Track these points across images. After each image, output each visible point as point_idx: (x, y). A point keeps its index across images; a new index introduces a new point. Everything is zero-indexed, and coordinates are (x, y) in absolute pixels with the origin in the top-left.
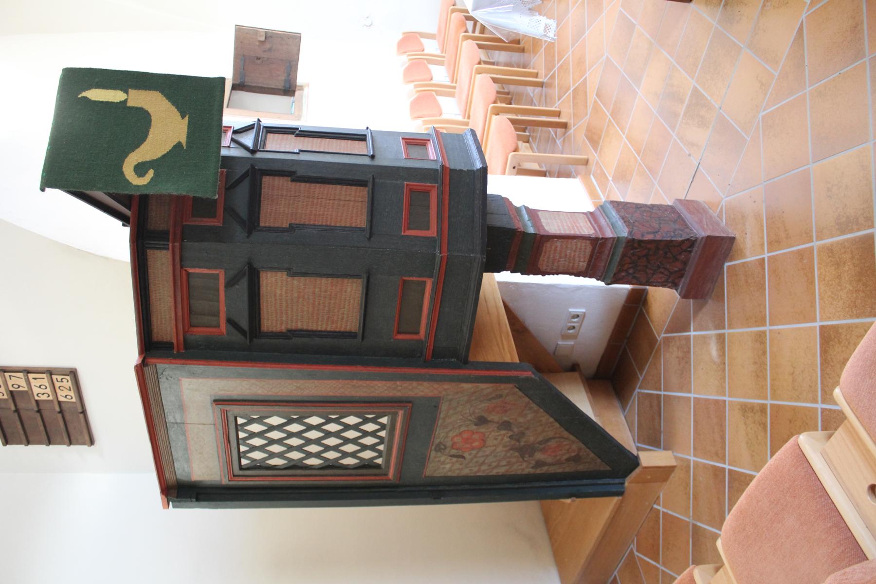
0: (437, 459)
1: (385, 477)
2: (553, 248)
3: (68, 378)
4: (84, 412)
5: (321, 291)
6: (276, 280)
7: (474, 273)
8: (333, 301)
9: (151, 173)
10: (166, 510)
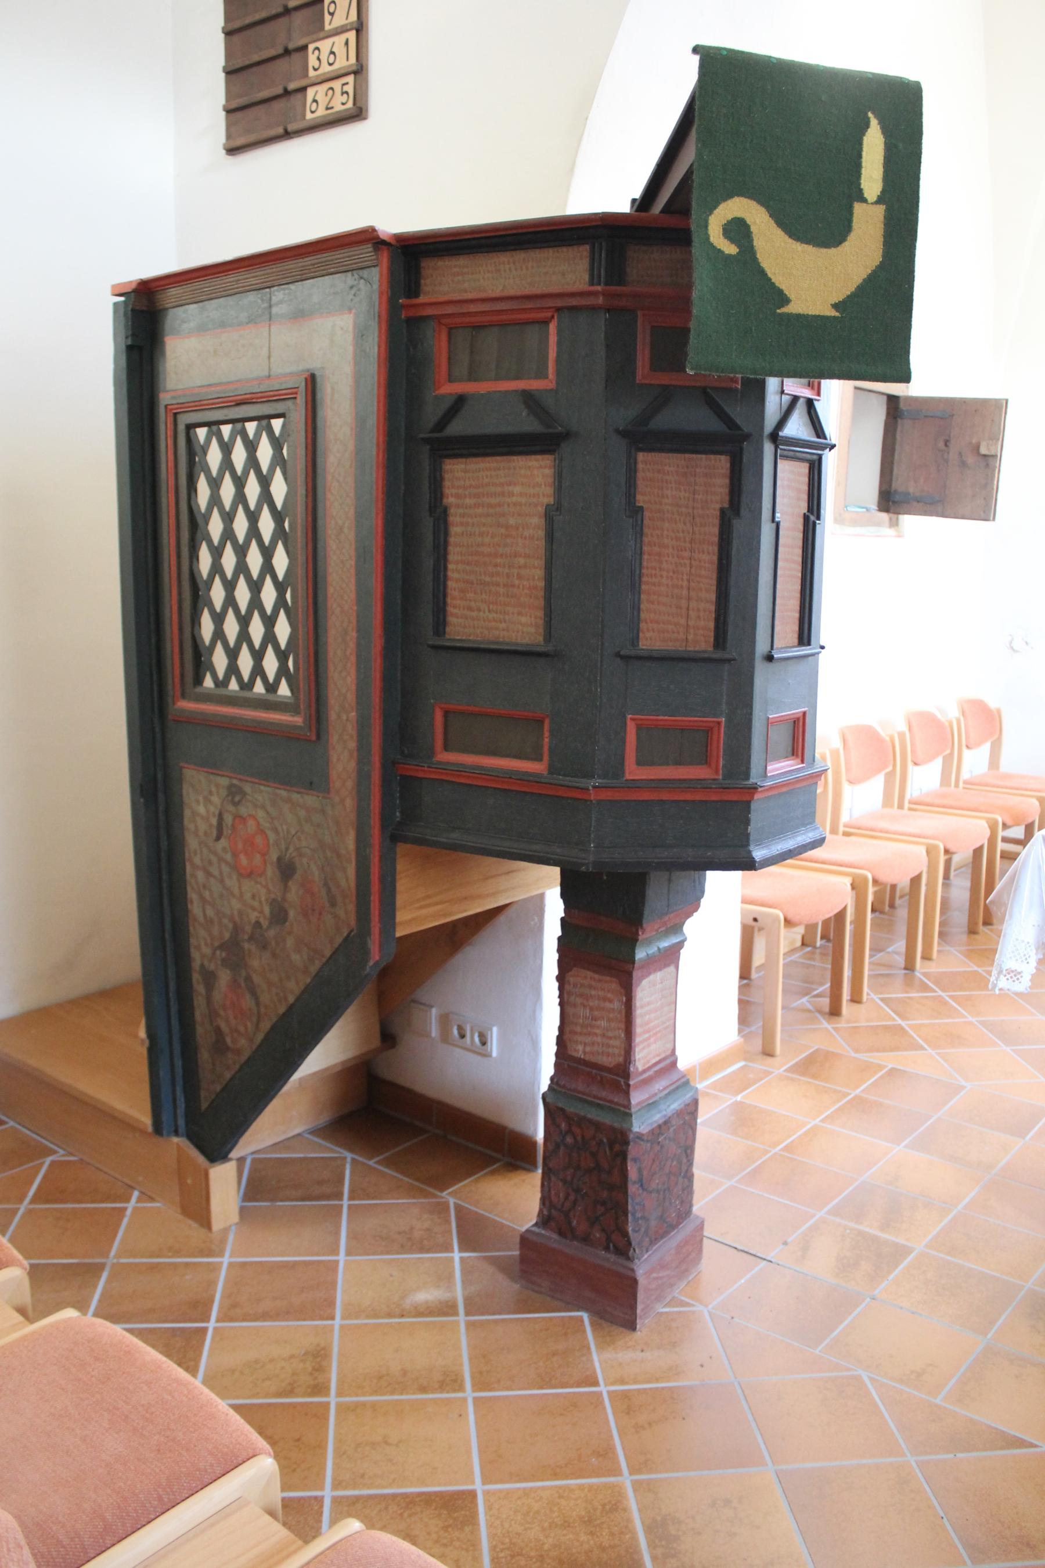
0: (214, 789)
1: (178, 693)
2: (609, 995)
3: (350, 105)
4: (287, 135)
5: (520, 567)
6: (538, 485)
7: (558, 850)
8: (501, 590)
9: (730, 249)
10: (108, 291)
